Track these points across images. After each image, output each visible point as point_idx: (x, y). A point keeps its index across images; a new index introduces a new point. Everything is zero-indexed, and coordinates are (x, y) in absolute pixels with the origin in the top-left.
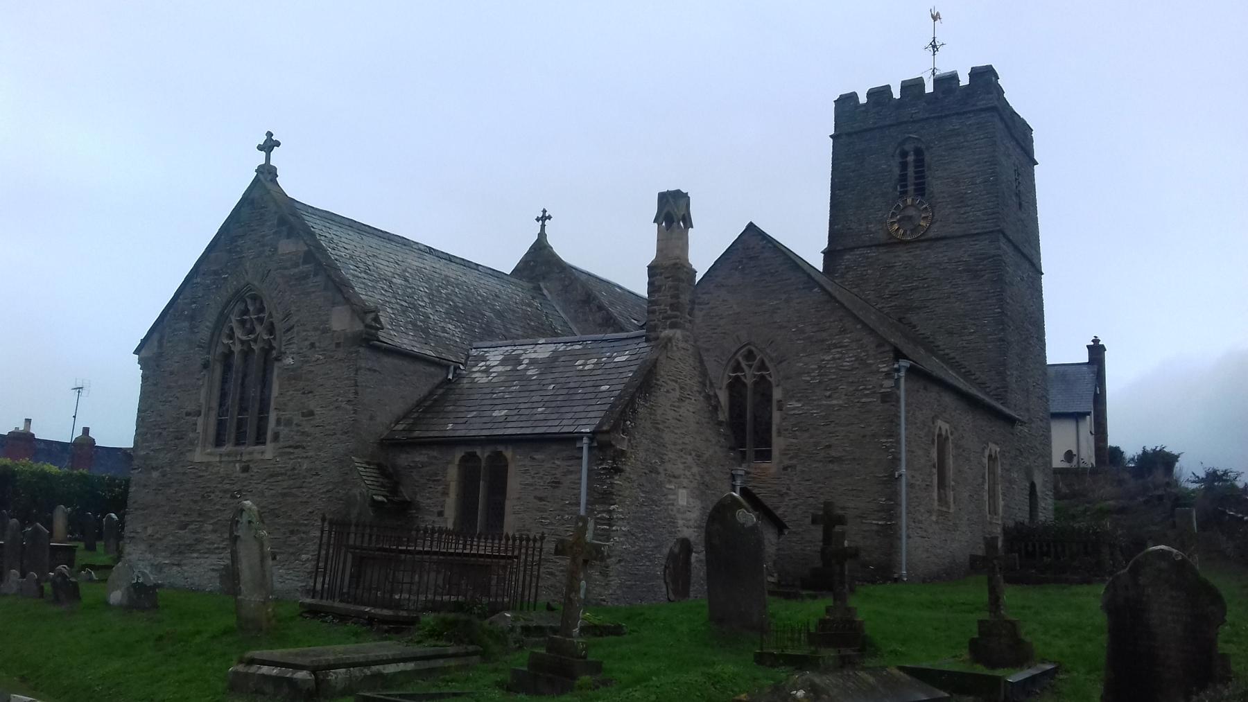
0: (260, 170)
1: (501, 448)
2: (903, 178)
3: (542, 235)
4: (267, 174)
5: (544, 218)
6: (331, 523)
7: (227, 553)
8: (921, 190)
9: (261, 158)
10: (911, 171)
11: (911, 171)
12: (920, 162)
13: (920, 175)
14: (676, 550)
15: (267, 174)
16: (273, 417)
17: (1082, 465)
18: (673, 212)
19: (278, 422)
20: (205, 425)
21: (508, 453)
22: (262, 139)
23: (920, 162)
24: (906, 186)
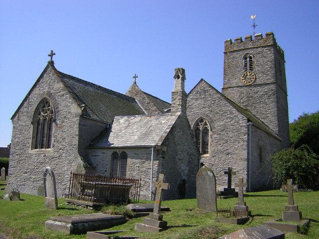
0: (49, 63)
1: (125, 150)
2: (246, 65)
3: (135, 83)
4: (51, 63)
5: (135, 77)
6: (74, 175)
7: (42, 182)
8: (251, 69)
9: (49, 59)
10: (248, 64)
11: (248, 64)
12: (251, 61)
13: (251, 65)
14: (181, 183)
15: (51, 63)
16: (53, 139)
17: (273, 80)
18: (180, 74)
19: (54, 142)
20: (30, 145)
21: (128, 152)
22: (50, 53)
23: (251, 61)
24: (250, 60)
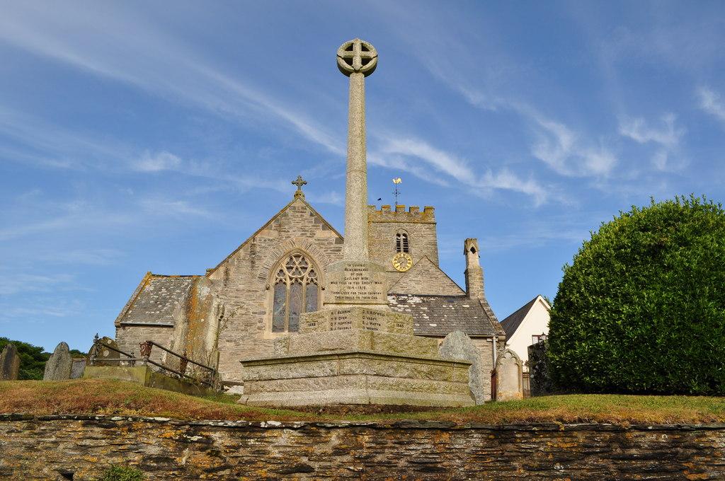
12: (405, 240)
